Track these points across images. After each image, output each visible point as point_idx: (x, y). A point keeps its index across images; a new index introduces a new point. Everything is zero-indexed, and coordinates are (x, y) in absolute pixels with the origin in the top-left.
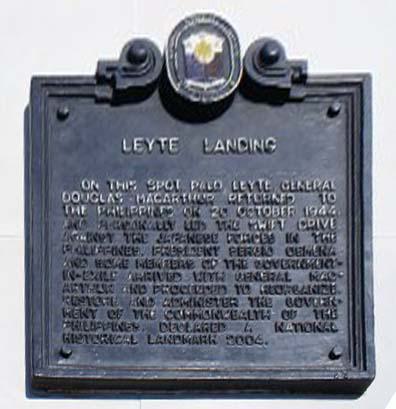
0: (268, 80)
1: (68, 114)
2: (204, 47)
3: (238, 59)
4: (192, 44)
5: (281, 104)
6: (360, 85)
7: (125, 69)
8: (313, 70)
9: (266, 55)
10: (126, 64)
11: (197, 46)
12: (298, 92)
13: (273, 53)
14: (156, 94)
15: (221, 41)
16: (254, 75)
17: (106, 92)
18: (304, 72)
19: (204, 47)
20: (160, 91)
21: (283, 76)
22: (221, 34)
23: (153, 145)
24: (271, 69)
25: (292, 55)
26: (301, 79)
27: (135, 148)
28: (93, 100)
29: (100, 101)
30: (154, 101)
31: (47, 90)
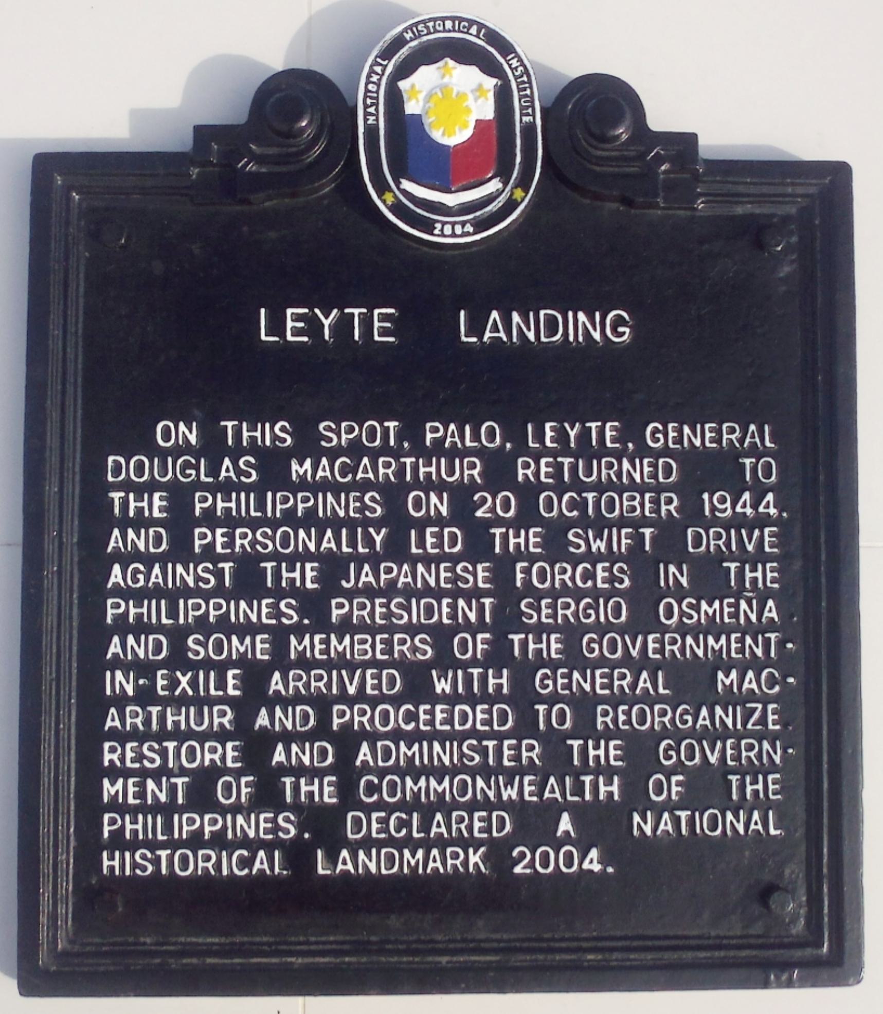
4: (421, 90)
22: (490, 68)
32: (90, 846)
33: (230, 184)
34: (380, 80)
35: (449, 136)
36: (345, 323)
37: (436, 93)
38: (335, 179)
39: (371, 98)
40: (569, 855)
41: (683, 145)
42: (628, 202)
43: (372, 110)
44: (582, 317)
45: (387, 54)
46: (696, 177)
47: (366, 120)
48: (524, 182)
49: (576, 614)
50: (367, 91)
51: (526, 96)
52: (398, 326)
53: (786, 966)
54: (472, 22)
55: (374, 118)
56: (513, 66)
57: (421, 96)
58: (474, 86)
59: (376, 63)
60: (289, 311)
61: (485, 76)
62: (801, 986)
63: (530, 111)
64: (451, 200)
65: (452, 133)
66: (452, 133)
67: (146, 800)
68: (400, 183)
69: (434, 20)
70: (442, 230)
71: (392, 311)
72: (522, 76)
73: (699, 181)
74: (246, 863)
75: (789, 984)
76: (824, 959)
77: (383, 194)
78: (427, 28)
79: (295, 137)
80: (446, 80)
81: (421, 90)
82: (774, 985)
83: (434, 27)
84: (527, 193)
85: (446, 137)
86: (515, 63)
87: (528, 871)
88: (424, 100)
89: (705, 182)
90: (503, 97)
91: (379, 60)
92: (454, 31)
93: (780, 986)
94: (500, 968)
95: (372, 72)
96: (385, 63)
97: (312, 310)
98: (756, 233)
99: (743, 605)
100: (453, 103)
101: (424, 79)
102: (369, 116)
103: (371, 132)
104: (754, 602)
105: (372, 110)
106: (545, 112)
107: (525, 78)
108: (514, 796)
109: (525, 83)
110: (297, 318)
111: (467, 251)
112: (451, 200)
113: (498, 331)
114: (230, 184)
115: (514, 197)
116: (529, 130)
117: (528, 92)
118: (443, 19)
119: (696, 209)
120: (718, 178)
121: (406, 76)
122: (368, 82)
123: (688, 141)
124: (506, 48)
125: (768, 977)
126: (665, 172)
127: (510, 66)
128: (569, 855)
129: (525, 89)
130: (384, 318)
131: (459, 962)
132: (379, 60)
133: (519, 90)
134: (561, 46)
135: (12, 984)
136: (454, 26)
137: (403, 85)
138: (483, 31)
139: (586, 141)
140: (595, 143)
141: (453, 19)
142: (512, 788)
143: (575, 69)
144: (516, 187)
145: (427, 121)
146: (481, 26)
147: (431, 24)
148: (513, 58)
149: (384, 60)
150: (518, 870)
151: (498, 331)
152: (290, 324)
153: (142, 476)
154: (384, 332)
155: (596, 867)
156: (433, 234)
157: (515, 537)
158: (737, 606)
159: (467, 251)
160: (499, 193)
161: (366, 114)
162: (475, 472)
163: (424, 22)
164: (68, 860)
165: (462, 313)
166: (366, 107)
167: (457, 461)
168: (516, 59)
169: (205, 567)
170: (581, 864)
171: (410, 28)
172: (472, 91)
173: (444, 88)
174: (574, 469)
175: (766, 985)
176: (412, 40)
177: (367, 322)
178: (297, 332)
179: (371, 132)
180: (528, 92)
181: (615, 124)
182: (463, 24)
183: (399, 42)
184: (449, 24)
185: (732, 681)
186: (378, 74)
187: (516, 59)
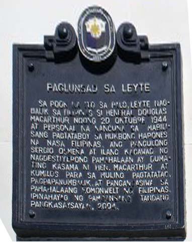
0: (130, 48)
1: (167, 67)
2: (95, 28)
3: (112, 34)
4: (91, 24)
5: (139, 63)
6: (174, 49)
7: (57, 41)
8: (152, 42)
9: (127, 32)
10: (58, 38)
11: (92, 26)
12: (144, 55)
13: (130, 31)
14: (118, 58)
15: (104, 23)
16: (122, 45)
17: (50, 54)
18: (146, 42)
19: (95, 28)
20: (120, 57)
21: (135, 45)
22: (104, 20)
23: (137, 88)
24: (129, 41)
25: (140, 33)
26: (146, 47)
27: (128, 90)
28: (45, 60)
29: (49, 60)
30: (119, 62)
31: (23, 53)
48: (111, 47)
152: (128, 88)
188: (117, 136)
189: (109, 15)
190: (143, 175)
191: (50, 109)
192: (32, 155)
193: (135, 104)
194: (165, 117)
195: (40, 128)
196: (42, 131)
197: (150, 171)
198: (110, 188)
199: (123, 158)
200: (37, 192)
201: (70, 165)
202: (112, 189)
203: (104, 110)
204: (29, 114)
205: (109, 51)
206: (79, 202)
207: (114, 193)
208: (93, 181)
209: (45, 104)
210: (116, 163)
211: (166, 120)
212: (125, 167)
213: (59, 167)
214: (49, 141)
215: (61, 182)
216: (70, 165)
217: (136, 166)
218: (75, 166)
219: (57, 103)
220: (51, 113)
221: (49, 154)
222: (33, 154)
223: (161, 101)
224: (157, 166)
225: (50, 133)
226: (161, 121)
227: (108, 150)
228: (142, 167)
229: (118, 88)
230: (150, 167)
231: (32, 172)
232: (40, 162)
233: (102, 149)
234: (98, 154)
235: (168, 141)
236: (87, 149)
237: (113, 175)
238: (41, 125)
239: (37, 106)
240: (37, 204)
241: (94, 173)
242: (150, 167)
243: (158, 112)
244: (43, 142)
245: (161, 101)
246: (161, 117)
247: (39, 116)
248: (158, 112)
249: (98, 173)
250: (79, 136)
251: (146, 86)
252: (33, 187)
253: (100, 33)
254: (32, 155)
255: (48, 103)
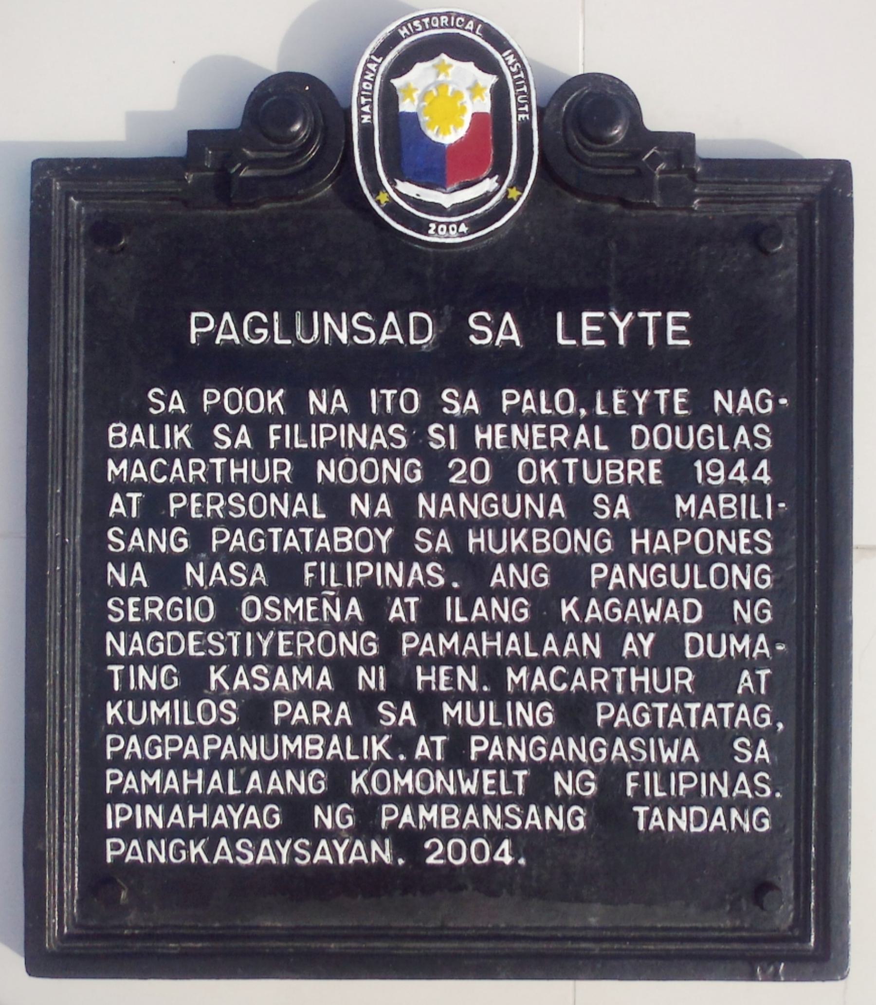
4: (417, 87)
9: (593, 109)
22: (487, 65)
32: (94, 832)
33: (224, 186)
34: (374, 78)
35: (444, 134)
36: (637, 329)
37: (431, 91)
38: (331, 180)
39: (366, 96)
40: (481, 848)
41: (681, 145)
42: (624, 203)
43: (366, 109)
44: (327, 317)
45: (382, 51)
46: (693, 176)
47: (360, 119)
48: (520, 182)
49: (163, 612)
50: (361, 89)
51: (523, 93)
52: (693, 329)
53: (773, 959)
54: (468, 18)
55: (369, 117)
56: (510, 63)
57: (415, 95)
58: (469, 82)
59: (370, 61)
60: (585, 315)
61: (480, 72)
62: (787, 979)
63: (526, 108)
64: (446, 199)
65: (448, 132)
66: (448, 132)
67: (517, 791)
68: (395, 184)
69: (430, 16)
70: (436, 230)
71: (686, 315)
72: (519, 73)
73: (697, 182)
74: (210, 851)
75: (775, 977)
76: (810, 953)
77: (378, 194)
78: (423, 24)
79: (605, 143)
80: (441, 77)
81: (417, 87)
82: (782, 979)
83: (430, 23)
84: (523, 191)
85: (441, 136)
86: (511, 59)
87: (441, 862)
88: (419, 97)
89: (702, 182)
90: (499, 94)
91: (373, 58)
92: (451, 27)
93: (765, 979)
94: (185, 955)
95: (366, 69)
96: (379, 60)
97: (607, 313)
98: (758, 236)
99: (326, 605)
100: (448, 101)
101: (420, 75)
102: (364, 113)
103: (366, 131)
104: (338, 601)
105: (366, 109)
106: (541, 112)
107: (522, 75)
108: (473, 791)
109: (522, 82)
110: (592, 321)
111: (451, 250)
112: (446, 199)
113: (395, 333)
114: (224, 186)
115: (509, 197)
116: (524, 128)
117: (525, 89)
118: (439, 15)
119: (693, 210)
120: (716, 179)
121: (401, 74)
122: (363, 80)
123: (686, 141)
124: (501, 44)
125: (755, 971)
126: (662, 172)
127: (506, 62)
128: (481, 848)
129: (521, 86)
130: (678, 321)
131: (648, 950)
132: (373, 58)
133: (517, 87)
134: (559, 44)
135: (19, 962)
136: (449, 22)
137: (397, 82)
138: (480, 26)
139: (580, 142)
140: (588, 143)
141: (448, 14)
142: (472, 782)
143: (575, 66)
144: (512, 187)
145: (424, 119)
146: (478, 22)
147: (426, 20)
148: (510, 54)
149: (378, 58)
150: (431, 860)
151: (395, 333)
152: (586, 328)
153: (263, 478)
154: (677, 335)
155: (508, 860)
156: (427, 234)
157: (637, 538)
158: (319, 604)
159: (451, 250)
160: (496, 192)
161: (361, 113)
162: (285, 473)
163: (420, 18)
164: (73, 846)
165: (560, 316)
166: (360, 106)
167: (267, 461)
168: (512, 56)
169: (238, 566)
170: (492, 854)
171: (405, 24)
172: (469, 89)
173: (440, 86)
174: (578, 469)
175: (752, 977)
176: (407, 36)
177: (661, 325)
178: (593, 336)
179: (366, 131)
180: (525, 89)
181: (612, 124)
182: (458, 19)
183: (394, 39)
184: (444, 20)
185: (522, 679)
186: (372, 72)
187: (512, 56)
188: (528, 540)
189: (510, 47)
190: (646, 716)
191: (202, 424)
192: (110, 637)
193: (617, 401)
194: (764, 464)
195: (154, 513)
196: (163, 522)
197: (680, 698)
198: (486, 773)
199: (550, 637)
200: (133, 799)
201: (295, 671)
202: (497, 777)
203: (466, 424)
204: (99, 452)
205: (507, 204)
206: (332, 835)
207: (504, 792)
208: (402, 741)
209: (177, 404)
210: (517, 662)
211: (766, 479)
212: (561, 678)
213: (241, 682)
214: (196, 567)
215: (251, 749)
216: (295, 671)
217: (614, 676)
218: (316, 675)
219: (234, 398)
220: (204, 446)
221: (196, 625)
222: (116, 630)
223: (745, 393)
224: (715, 680)
225: (200, 532)
226: (743, 478)
227: (480, 601)
228: (646, 679)
229: (536, 327)
230: (683, 678)
231: (112, 712)
232: (149, 663)
233: (454, 593)
234: (432, 619)
235: (774, 571)
236: (375, 598)
237: (501, 714)
238: (155, 500)
239: (137, 414)
240: (133, 852)
241: (407, 705)
242: (683, 678)
243: (729, 441)
244: (165, 575)
245: (745, 393)
246: (741, 463)
247: (147, 456)
248: (729, 441)
249: (428, 705)
250: (345, 538)
251: (674, 327)
252: (112, 778)
253: (467, 119)
254: (110, 637)
255: (193, 401)
